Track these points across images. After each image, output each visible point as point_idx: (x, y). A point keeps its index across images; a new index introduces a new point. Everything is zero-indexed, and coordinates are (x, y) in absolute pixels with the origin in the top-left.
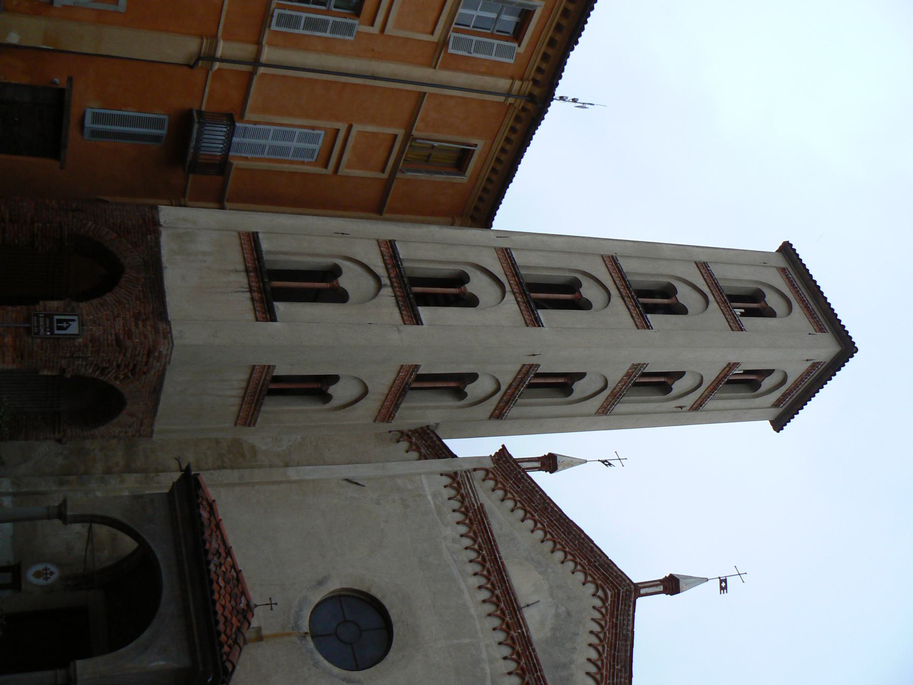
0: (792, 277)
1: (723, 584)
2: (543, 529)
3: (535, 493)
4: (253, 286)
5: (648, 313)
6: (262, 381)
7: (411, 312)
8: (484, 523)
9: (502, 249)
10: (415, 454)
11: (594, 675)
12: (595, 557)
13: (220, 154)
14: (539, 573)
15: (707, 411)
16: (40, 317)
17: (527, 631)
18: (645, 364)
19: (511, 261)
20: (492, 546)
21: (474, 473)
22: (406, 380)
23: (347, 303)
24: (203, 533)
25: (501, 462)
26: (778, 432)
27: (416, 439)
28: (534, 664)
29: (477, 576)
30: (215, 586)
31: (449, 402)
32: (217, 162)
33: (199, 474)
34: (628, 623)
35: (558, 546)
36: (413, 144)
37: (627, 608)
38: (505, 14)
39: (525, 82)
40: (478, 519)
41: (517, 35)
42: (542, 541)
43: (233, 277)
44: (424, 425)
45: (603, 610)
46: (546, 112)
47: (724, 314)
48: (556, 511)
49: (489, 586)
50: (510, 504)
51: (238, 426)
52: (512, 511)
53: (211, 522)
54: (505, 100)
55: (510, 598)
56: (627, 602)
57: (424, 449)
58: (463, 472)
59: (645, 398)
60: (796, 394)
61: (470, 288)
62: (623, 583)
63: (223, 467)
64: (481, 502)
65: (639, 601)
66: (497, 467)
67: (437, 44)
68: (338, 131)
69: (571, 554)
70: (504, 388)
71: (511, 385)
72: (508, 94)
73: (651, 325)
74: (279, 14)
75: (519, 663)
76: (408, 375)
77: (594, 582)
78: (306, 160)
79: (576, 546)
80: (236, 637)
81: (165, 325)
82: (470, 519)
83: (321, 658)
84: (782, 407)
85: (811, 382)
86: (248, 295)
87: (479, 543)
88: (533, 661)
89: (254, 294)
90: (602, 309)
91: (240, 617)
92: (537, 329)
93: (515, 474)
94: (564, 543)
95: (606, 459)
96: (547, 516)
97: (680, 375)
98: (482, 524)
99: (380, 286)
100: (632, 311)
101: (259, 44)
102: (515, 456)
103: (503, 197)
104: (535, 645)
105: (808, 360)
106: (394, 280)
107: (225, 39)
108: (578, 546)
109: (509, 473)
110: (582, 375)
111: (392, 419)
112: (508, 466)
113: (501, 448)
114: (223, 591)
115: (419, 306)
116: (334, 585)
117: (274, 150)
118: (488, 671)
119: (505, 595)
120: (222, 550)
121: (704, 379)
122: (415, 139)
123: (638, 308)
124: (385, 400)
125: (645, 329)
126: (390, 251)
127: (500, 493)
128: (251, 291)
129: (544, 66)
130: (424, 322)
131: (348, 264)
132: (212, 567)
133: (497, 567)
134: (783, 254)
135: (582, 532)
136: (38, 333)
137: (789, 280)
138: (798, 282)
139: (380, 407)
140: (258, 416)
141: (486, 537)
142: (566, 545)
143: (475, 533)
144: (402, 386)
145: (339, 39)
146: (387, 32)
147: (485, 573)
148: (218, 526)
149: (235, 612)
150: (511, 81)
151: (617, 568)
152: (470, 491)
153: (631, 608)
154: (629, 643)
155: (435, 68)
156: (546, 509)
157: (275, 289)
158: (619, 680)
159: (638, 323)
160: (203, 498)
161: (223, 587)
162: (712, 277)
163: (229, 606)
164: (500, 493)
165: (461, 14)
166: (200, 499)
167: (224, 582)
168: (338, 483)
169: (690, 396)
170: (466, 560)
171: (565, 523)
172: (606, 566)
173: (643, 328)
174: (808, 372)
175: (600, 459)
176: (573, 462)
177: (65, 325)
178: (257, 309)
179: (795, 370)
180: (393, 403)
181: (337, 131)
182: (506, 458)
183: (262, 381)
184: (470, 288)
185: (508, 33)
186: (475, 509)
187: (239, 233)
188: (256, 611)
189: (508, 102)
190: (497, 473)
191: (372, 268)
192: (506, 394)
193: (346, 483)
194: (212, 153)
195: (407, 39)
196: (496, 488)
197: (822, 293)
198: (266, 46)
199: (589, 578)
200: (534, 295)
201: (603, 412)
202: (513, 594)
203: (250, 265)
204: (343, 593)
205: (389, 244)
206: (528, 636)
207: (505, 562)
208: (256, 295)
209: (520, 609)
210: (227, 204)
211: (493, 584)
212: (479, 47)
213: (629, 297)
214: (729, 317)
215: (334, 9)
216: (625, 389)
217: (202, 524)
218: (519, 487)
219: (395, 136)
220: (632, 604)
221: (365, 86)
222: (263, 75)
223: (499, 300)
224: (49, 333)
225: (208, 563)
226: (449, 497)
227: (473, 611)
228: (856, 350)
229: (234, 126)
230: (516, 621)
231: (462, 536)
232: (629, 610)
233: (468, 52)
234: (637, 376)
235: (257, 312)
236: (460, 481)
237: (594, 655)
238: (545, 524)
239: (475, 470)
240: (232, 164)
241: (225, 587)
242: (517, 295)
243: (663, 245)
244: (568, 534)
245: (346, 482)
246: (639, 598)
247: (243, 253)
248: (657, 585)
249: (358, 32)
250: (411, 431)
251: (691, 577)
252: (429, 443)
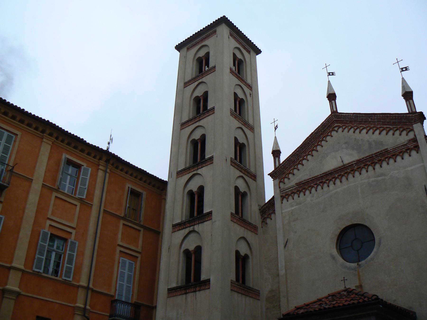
0: (191, 45)
1: (331, 74)
2: (307, 155)
6: (238, 286)
8: (304, 183)
9: (177, 175)
10: (273, 216)
11: (374, 130)
12: (320, 131)
13: (130, 307)
14: (327, 157)
15: (254, 124)
17: (354, 161)
18: (230, 110)
19: (182, 171)
20: (315, 179)
21: (281, 188)
22: (237, 219)
24: (311, 311)
25: (276, 175)
26: (261, 52)
27: (265, 215)
28: (369, 158)
29: (329, 186)
30: (336, 305)
31: (248, 200)
33: (283, 314)
34: (350, 116)
35: (315, 148)
36: (127, 216)
37: (342, 116)
38: (68, 171)
39: (100, 164)
40: (302, 185)
41: (78, 166)
42: (313, 156)
45: (344, 127)
46: (114, 154)
47: (208, 75)
48: (299, 150)
49: (334, 180)
50: (295, 171)
52: (298, 170)
53: (306, 308)
54: (108, 173)
55: (339, 170)
56: (340, 117)
57: (270, 211)
60: (244, 44)
61: (195, 190)
62: (331, 119)
63: (280, 305)
65: (339, 111)
66: (278, 177)
67: (81, 203)
68: (120, 251)
70: (242, 174)
71: (240, 171)
72: (105, 172)
73: (213, 107)
74: (64, 277)
75: (369, 165)
77: (331, 132)
78: (134, 266)
79: (314, 140)
80: (360, 295)
82: (303, 189)
83: (369, 257)
86: (197, 293)
88: (368, 159)
91: (350, 294)
92: (214, 159)
93: (282, 169)
94: (313, 146)
95: (274, 128)
97: (235, 94)
99: (194, 231)
101: (78, 287)
102: (273, 169)
103: (153, 175)
104: (361, 158)
105: (229, 38)
107: (76, 303)
109: (281, 171)
110: (236, 139)
111: (256, 226)
112: (278, 172)
113: (269, 175)
114: (338, 302)
115: (203, 212)
116: (335, 252)
117: (129, 282)
118: (373, 179)
119: (338, 172)
120: (319, 303)
121: (237, 84)
122: (125, 215)
123: (205, 113)
124: (247, 229)
125: (214, 110)
126: (177, 227)
127: (290, 176)
128: (195, 291)
129: (93, 155)
130: (211, 210)
131: (183, 246)
132: (327, 307)
133: (325, 176)
134: (181, 49)
135: (308, 138)
137: (193, 46)
138: (194, 42)
139: (251, 232)
140: (255, 289)
142: (314, 145)
143: (309, 187)
144: (241, 221)
145: (77, 249)
146: (75, 227)
147: (327, 182)
148: (307, 305)
149: (348, 296)
150: (99, 170)
151: (324, 121)
152: (289, 190)
153: (343, 115)
154: (359, 115)
155: (92, 205)
156: (297, 154)
157: (195, 280)
158: (376, 119)
159: (212, 113)
160: (294, 312)
161: (336, 302)
162: (191, 80)
163: (345, 299)
164: (290, 176)
165: (68, 191)
166: (295, 313)
167: (334, 301)
168: (286, 251)
169: (245, 90)
170: (322, 190)
171: (304, 146)
172: (323, 126)
173: (214, 111)
174: (234, 38)
175: (274, 130)
176: (276, 143)
179: (234, 43)
181: (121, 251)
182: (274, 173)
183: (238, 286)
184: (195, 190)
185: (77, 171)
186: (298, 187)
187: (168, 297)
188: (347, 287)
189: (109, 172)
190: (281, 177)
191: (185, 235)
195: (79, 217)
196: (288, 178)
198: (79, 283)
199: (329, 134)
200: (199, 160)
202: (337, 168)
203: (183, 292)
204: (338, 247)
206: (356, 161)
207: (322, 173)
208: (198, 289)
209: (344, 165)
210: (154, 305)
211: (333, 178)
212: (83, 184)
213: (200, 118)
214: (209, 72)
215: (63, 251)
216: (242, 119)
217: (306, 312)
218: (288, 167)
219: (124, 224)
220: (341, 114)
221: (100, 238)
222: (93, 285)
223: (200, 176)
225: (325, 308)
226: (292, 199)
227: (346, 187)
230: (350, 167)
231: (310, 193)
232: (344, 116)
233: (86, 189)
235: (206, 288)
236: (285, 194)
237: (364, 131)
238: (305, 155)
239: (280, 188)
240: (135, 302)
241: (336, 301)
242: (198, 168)
244: (309, 144)
245: (286, 247)
246: (338, 111)
247: (177, 295)
248: (332, 104)
249: (75, 240)
250: (262, 218)
251: (328, 88)
252: (267, 209)
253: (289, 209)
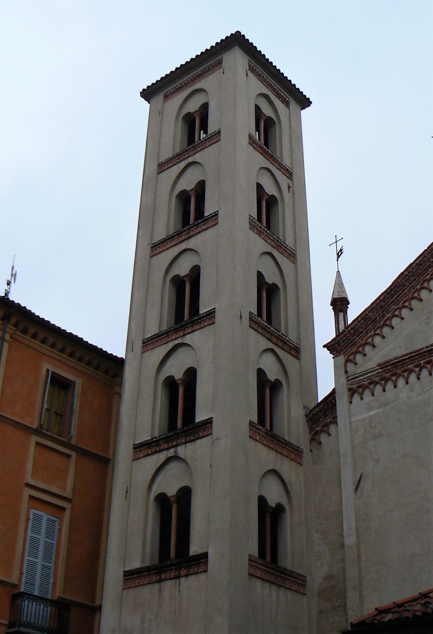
2: (400, 309)
3: (367, 317)
4: (174, 575)
5: (204, 215)
6: (263, 568)
7: (201, 428)
9: (143, 346)
10: (332, 427)
12: (426, 261)
13: (49, 608)
15: (292, 164)
18: (250, 218)
19: (154, 338)
20: (416, 355)
23: (192, 488)
24: (407, 618)
25: (339, 348)
26: (311, 103)
31: (284, 396)
32: (57, 611)
33: (351, 623)
36: (45, 427)
42: (412, 309)
43: (166, 593)
44: (305, 419)
46: (19, 304)
47: (205, 148)
48: (384, 298)
50: (377, 340)
51: (305, 592)
52: (384, 337)
53: (396, 612)
54: (6, 341)
57: (327, 419)
58: (349, 383)
59: (280, 220)
60: (277, 86)
61: (178, 375)
63: (345, 605)
64: (376, 366)
68: (31, 497)
69: (423, 283)
70: (271, 346)
71: (268, 339)
76: (258, 431)
78: (57, 527)
79: (415, 279)
82: (393, 375)
84: (289, 99)
85: (267, 73)
86: (182, 580)
87: (414, 366)
89: (182, 574)
90: (199, 255)
92: (217, 314)
93: (350, 335)
94: (413, 290)
96: (388, 306)
98: (396, 365)
99: (176, 458)
100: (201, 229)
103: (96, 347)
105: (247, 75)
106: (170, 445)
108: (415, 277)
110: (260, 275)
112: (343, 342)
113: (326, 348)
117: (47, 557)
120: (423, 601)
122: (41, 426)
123: (199, 223)
124: (281, 454)
125: (218, 217)
127: (367, 349)
128: (178, 577)
131: (155, 487)
134: (151, 97)
135: (402, 274)
137: (176, 92)
138: (177, 84)
139: (288, 459)
141: (408, 361)
143: (404, 371)
148: (400, 605)
152: (366, 376)
156: (382, 307)
159: (213, 224)
160: (374, 619)
173: (217, 219)
174: (258, 75)
175: (336, 259)
176: (339, 283)
178: (195, 571)
180: (285, 448)
182: (335, 344)
183: (263, 568)
184: (178, 375)
186: (383, 372)
187: (124, 589)
192: (277, 343)
193: (359, 491)
194: (48, 616)
197: (187, 62)
200: (186, 317)
201: (293, 257)
205: (137, 450)
208: (183, 572)
210: (97, 603)
213: (189, 233)
214: (208, 144)
216: (272, 237)
217: (398, 619)
218: (362, 332)
219: (38, 444)
223: (190, 348)
228: (238, 32)
229: (22, 592)
234: (260, 225)
238: (396, 307)
239: (346, 372)
240: (59, 597)
242: (186, 332)
243: (142, 203)
245: (358, 491)
252: (321, 415)
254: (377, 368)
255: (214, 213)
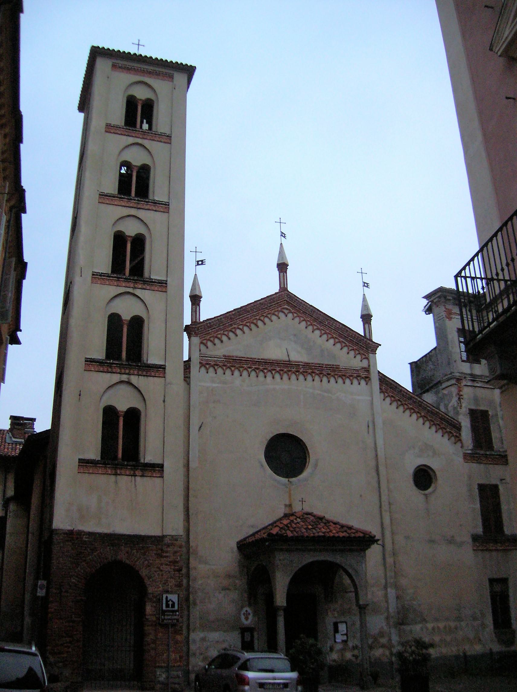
16: (164, 618)
40: (232, 361)
61: (126, 316)
81: (166, 539)
131: (104, 398)
136: (178, 620)
153: (306, 304)
177: (170, 603)
207: (262, 358)
224: (177, 613)
253: (208, 384)
254: (222, 357)
255: (165, 202)
